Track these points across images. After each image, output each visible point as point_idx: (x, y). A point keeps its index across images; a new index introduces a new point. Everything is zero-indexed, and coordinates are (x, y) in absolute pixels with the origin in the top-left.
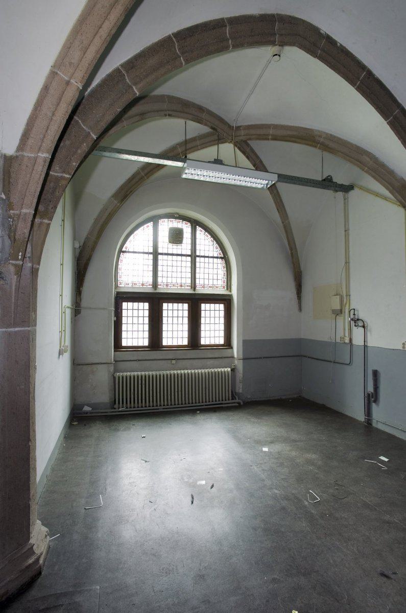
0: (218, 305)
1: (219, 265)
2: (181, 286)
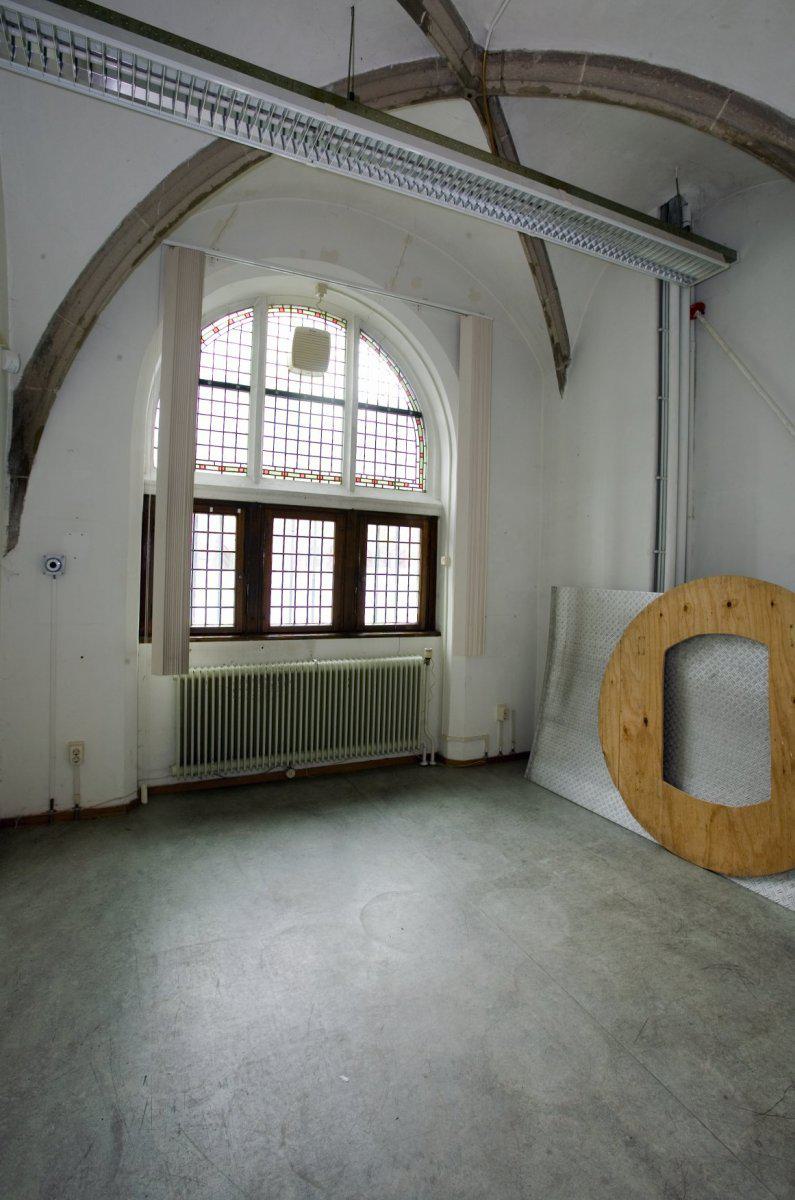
0: (319, 523)
1: (411, 431)
2: (320, 478)
